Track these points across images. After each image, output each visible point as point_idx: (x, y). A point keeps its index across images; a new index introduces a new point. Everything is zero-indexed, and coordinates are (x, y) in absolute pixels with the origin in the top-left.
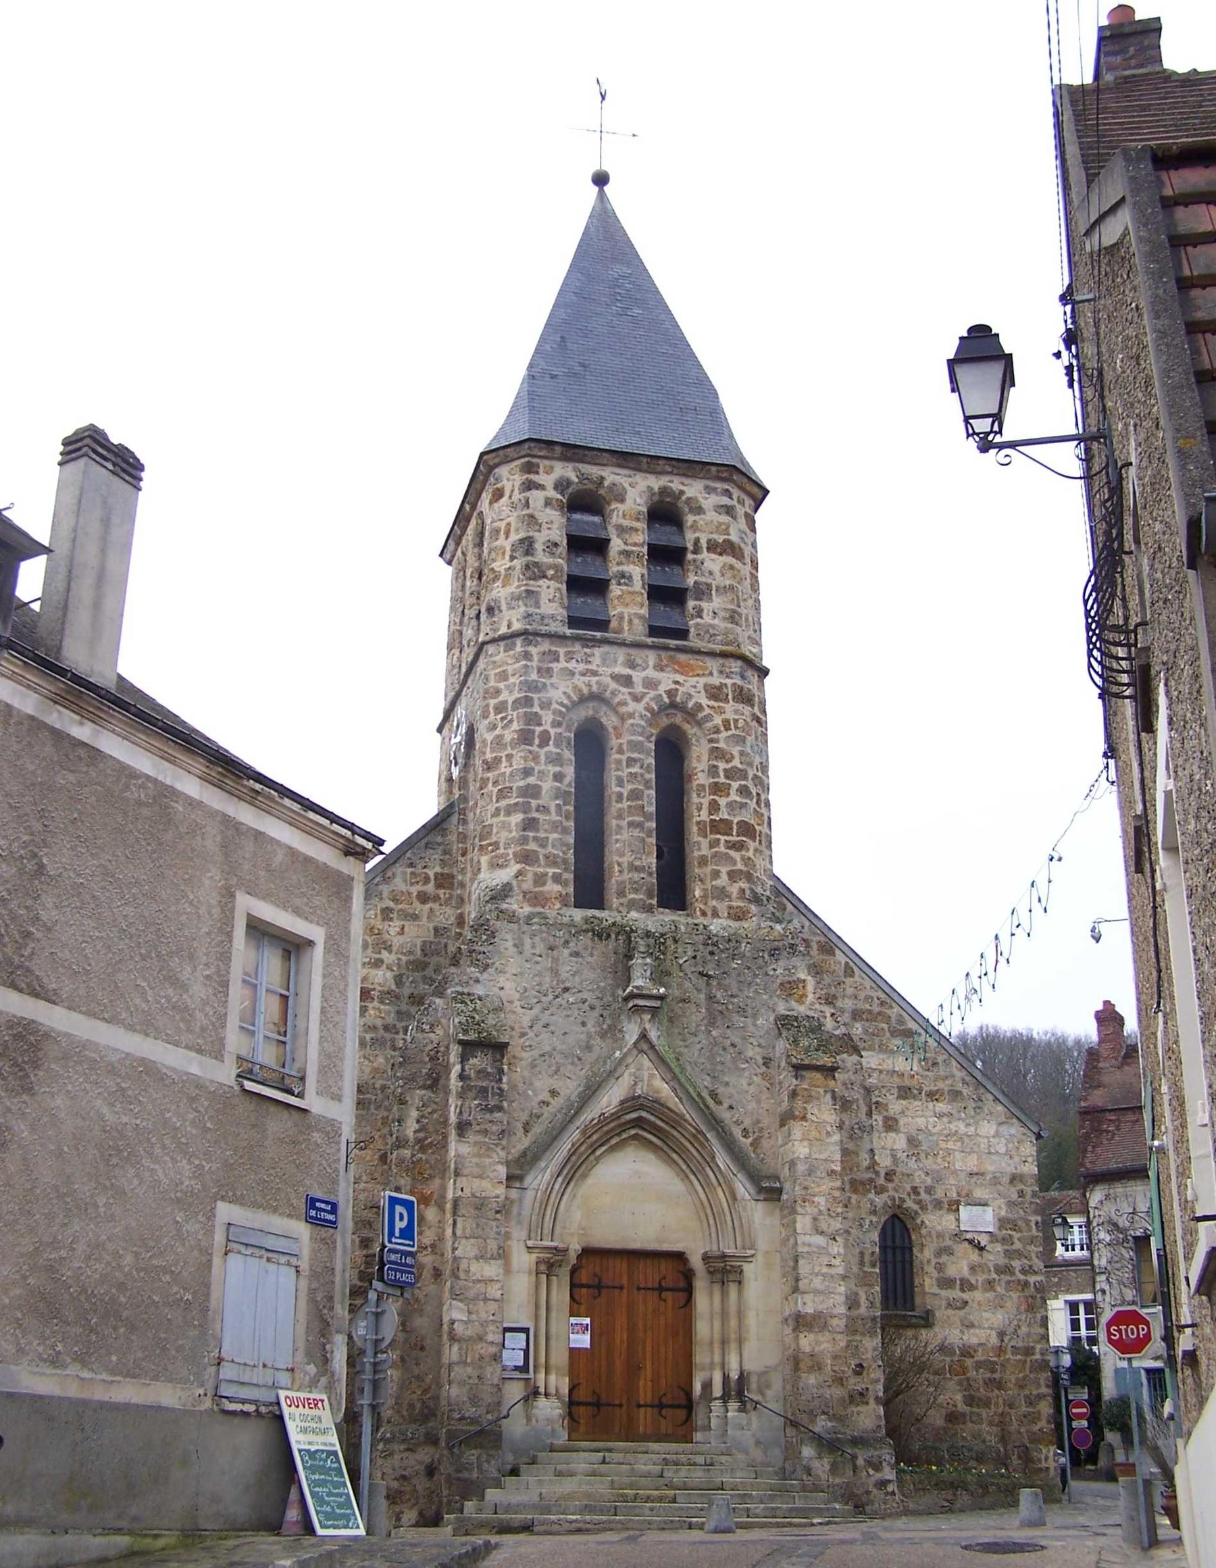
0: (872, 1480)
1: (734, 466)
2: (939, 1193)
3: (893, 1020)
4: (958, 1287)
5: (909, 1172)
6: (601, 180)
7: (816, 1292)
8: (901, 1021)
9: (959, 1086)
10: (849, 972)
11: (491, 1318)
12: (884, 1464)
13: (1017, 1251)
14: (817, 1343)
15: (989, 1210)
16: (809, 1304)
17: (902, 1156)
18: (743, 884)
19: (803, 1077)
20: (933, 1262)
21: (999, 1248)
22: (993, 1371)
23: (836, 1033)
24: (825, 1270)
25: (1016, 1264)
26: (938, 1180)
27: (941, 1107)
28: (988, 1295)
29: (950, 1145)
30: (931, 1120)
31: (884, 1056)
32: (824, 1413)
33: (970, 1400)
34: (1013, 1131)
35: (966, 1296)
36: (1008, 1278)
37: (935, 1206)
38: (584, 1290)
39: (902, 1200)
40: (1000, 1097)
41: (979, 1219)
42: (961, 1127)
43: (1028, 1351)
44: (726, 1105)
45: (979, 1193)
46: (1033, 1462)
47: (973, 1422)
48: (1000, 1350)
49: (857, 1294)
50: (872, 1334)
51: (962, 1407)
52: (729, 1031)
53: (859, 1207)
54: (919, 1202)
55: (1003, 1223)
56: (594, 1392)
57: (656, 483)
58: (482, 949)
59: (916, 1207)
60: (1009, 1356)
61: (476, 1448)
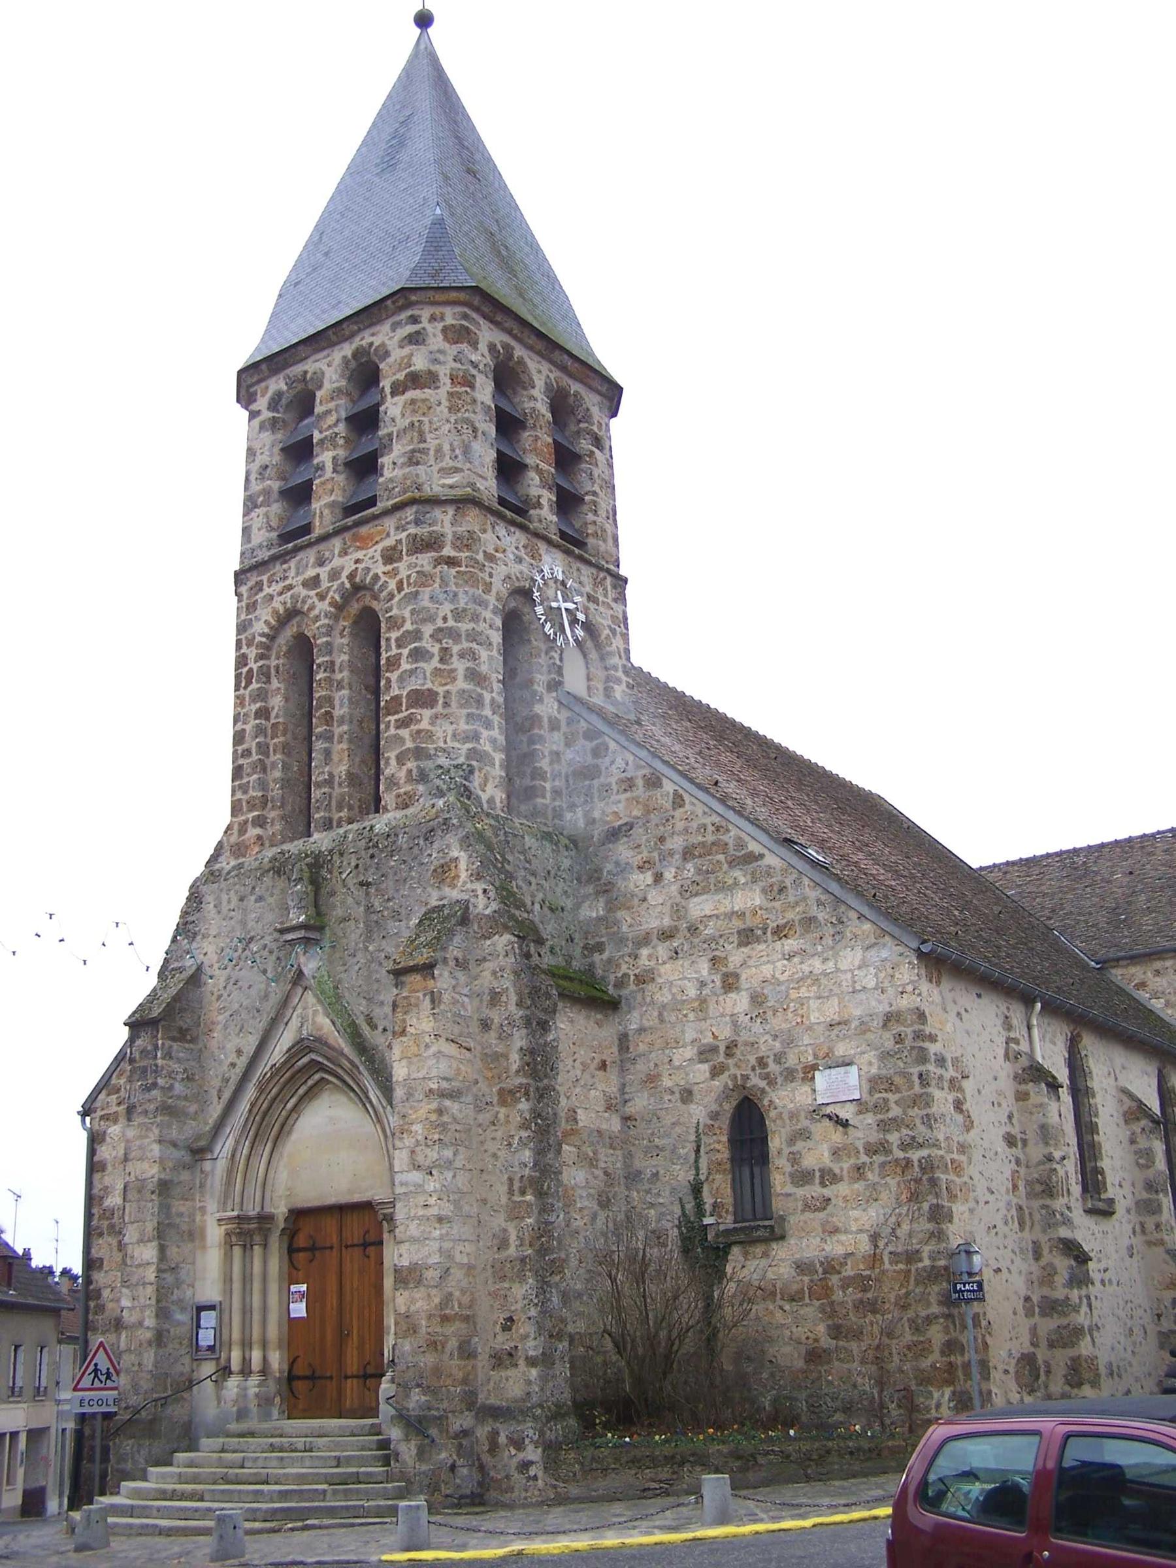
0: (514, 1462)
1: (403, 289)
2: (791, 1061)
3: (731, 847)
4: (817, 1181)
6: (424, 20)
7: (413, 1240)
8: (740, 844)
9: (814, 911)
11: (148, 1302)
12: (527, 1441)
13: (894, 1119)
14: (413, 1301)
15: (854, 1069)
16: (405, 1255)
18: (411, 765)
19: (403, 983)
20: (786, 1151)
21: (870, 1119)
22: (865, 1290)
23: (487, 912)
24: (421, 1213)
25: (894, 1138)
26: (790, 1042)
27: (791, 944)
28: (856, 1186)
29: (804, 992)
30: (779, 964)
31: (721, 896)
32: (418, 1386)
33: (836, 1332)
34: (884, 954)
35: (826, 1192)
36: (882, 1159)
37: (786, 1078)
38: (301, 1254)
39: (746, 1078)
40: (865, 911)
41: (839, 1086)
42: (817, 965)
43: (912, 1257)
44: (380, 1028)
45: (842, 1050)
46: (918, 1411)
47: (839, 1360)
48: (874, 1259)
49: (505, 1230)
50: (522, 1279)
51: (826, 1342)
52: (384, 942)
53: (508, 1122)
54: (766, 1077)
55: (875, 1083)
56: (310, 1365)
57: (347, 349)
58: (193, 918)
59: (763, 1084)
61: (131, 1438)
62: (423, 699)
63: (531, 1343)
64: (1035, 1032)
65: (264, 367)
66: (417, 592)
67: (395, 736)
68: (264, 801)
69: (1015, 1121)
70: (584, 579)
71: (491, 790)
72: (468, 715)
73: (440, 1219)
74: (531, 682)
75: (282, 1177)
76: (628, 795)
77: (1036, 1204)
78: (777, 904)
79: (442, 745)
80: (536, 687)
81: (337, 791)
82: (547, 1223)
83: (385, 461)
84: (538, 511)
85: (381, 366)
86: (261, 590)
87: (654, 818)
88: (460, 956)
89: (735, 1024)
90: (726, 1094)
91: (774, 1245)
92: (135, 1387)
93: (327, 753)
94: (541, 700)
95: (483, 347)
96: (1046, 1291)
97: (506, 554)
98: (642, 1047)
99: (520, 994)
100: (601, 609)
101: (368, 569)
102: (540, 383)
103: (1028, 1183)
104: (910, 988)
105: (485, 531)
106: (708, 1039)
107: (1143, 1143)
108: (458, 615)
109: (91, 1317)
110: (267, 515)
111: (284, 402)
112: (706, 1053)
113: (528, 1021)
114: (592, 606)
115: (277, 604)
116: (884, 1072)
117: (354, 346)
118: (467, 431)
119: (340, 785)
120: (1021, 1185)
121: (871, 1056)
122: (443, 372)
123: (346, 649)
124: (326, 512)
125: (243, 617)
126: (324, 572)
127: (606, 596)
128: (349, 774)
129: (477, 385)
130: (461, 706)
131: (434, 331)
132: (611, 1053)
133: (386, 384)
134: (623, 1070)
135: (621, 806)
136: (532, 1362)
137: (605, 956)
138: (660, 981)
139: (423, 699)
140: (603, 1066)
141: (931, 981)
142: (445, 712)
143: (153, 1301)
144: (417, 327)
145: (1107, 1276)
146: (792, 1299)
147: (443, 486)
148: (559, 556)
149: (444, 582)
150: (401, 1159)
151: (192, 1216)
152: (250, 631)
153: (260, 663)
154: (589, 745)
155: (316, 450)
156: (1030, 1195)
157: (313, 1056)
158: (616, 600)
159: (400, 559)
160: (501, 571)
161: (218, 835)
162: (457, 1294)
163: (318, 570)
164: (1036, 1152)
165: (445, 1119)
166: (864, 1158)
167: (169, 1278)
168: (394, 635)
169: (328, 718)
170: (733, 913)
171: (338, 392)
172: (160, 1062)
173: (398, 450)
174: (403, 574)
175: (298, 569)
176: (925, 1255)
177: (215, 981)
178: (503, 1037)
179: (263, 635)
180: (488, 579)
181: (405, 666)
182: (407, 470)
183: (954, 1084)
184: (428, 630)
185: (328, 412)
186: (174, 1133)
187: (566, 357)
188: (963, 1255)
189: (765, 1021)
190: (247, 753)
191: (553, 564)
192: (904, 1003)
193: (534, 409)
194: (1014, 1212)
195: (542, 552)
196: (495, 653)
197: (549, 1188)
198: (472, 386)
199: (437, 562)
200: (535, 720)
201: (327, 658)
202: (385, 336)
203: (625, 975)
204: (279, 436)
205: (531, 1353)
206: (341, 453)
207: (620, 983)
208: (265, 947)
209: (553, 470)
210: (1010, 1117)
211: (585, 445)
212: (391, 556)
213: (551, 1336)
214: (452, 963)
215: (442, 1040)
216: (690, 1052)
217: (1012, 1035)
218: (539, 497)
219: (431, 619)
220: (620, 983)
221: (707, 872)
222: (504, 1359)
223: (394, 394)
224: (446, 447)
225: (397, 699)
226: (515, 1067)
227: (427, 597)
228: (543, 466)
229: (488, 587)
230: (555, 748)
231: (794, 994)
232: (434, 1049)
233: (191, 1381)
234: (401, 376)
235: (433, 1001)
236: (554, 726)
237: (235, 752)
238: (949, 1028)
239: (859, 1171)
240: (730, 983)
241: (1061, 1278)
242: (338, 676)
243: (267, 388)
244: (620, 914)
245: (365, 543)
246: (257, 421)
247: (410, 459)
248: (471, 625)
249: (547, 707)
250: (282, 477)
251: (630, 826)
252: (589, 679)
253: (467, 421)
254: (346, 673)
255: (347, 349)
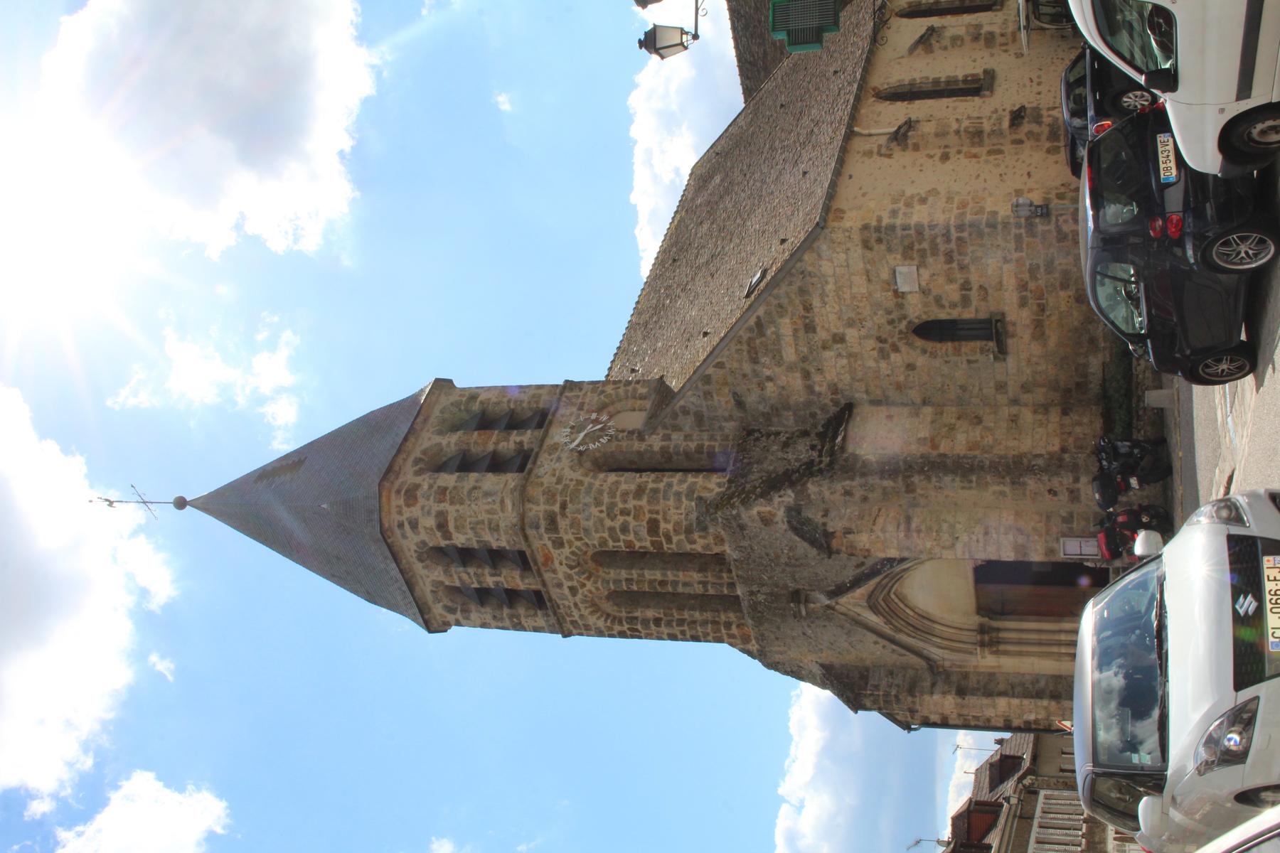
2: (890, 304)
8: (750, 329)
9: (795, 287)
15: (899, 269)
20: (948, 310)
21: (930, 260)
25: (942, 247)
27: (816, 303)
29: (847, 296)
35: (975, 287)
41: (908, 277)
45: (885, 275)
54: (900, 320)
55: (907, 255)
62: (653, 527)
64: (873, 131)
68: (715, 623)
69: (932, 153)
71: (712, 486)
73: (986, 533)
74: (639, 452)
75: (956, 619)
77: (986, 140)
78: (790, 309)
81: (710, 579)
82: (990, 467)
83: (495, 545)
87: (730, 379)
89: (866, 337)
91: (1008, 319)
93: (685, 584)
94: (650, 446)
95: (418, 480)
98: (879, 392)
99: (845, 479)
102: (438, 439)
103: (973, 145)
105: (542, 484)
106: (875, 353)
107: (946, 42)
108: (598, 503)
110: (527, 617)
111: (450, 604)
112: (883, 355)
114: (586, 407)
115: (586, 612)
116: (900, 251)
118: (475, 493)
121: (890, 258)
122: (436, 507)
126: (567, 584)
128: (700, 571)
131: (408, 513)
133: (443, 543)
136: (1077, 480)
137: (819, 412)
139: (653, 527)
146: (1043, 310)
149: (578, 511)
151: (979, 674)
154: (681, 417)
155: (484, 585)
156: (981, 144)
158: (581, 389)
160: (568, 474)
161: (735, 652)
164: (952, 139)
165: (923, 527)
166: (955, 265)
167: (1018, 689)
168: (611, 543)
171: (445, 572)
174: (571, 537)
177: (828, 657)
178: (872, 488)
181: (631, 537)
184: (608, 523)
185: (460, 578)
186: (927, 684)
189: (864, 319)
190: (683, 633)
191: (559, 435)
192: (856, 237)
194: (991, 158)
196: (622, 479)
198: (446, 489)
199: (564, 515)
200: (664, 450)
202: (409, 544)
203: (832, 400)
206: (487, 571)
207: (836, 403)
210: (930, 157)
212: (559, 544)
215: (875, 528)
216: (883, 365)
217: (875, 150)
219: (601, 521)
220: (836, 403)
225: (653, 543)
229: (580, 483)
231: (848, 302)
232: (880, 534)
234: (439, 534)
236: (667, 438)
238: (872, 205)
239: (962, 268)
240: (839, 339)
242: (635, 576)
244: (792, 403)
245: (548, 559)
246: (462, 621)
248: (605, 495)
249: (656, 442)
250: (500, 607)
251: (735, 394)
252: (634, 410)
253: (470, 492)
255: (418, 568)
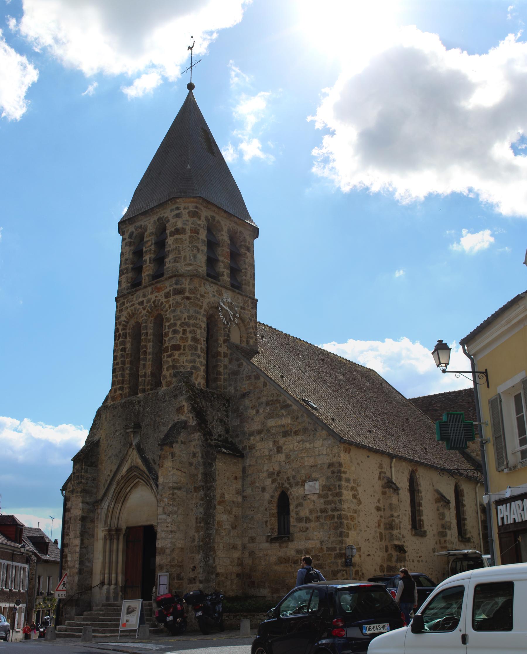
3: (281, 401)
5: (285, 471)
6: (191, 87)
7: (162, 539)
8: (285, 401)
10: (265, 385)
14: (162, 559)
17: (283, 464)
21: (322, 500)
24: (165, 529)
25: (329, 507)
27: (299, 438)
29: (303, 455)
30: (295, 444)
35: (307, 525)
41: (313, 488)
45: (314, 475)
49: (194, 536)
54: (289, 484)
57: (155, 218)
59: (288, 486)
60: (325, 552)
62: (176, 347)
63: (200, 575)
64: (393, 469)
65: (127, 222)
66: (175, 309)
67: (166, 360)
68: (123, 382)
70: (240, 301)
71: (199, 380)
72: (192, 353)
74: (217, 340)
75: (124, 516)
76: (248, 382)
79: (182, 364)
80: (219, 341)
81: (148, 379)
83: (167, 260)
84: (222, 277)
85: (167, 225)
86: (124, 305)
88: (183, 440)
89: (280, 465)
90: (276, 489)
91: (290, 543)
92: (72, 589)
93: (144, 365)
94: (221, 346)
95: (203, 218)
96: (389, 563)
97: (209, 292)
98: (250, 472)
100: (246, 312)
101: (160, 300)
102: (225, 229)
103: (385, 524)
104: (337, 454)
105: (200, 287)
106: (271, 470)
107: (441, 510)
108: (189, 317)
109: (63, 564)
110: (127, 277)
112: (270, 475)
113: (204, 463)
114: (242, 311)
115: (129, 310)
116: (327, 484)
117: (158, 217)
119: (148, 377)
120: (382, 525)
122: (188, 228)
123: (152, 328)
124: (147, 278)
125: (118, 314)
126: (145, 300)
127: (248, 306)
128: (152, 373)
129: (200, 233)
130: (190, 350)
132: (239, 474)
133: (168, 232)
134: (243, 480)
135: (246, 385)
136: (201, 582)
137: (239, 439)
138: (257, 448)
139: (176, 347)
140: (236, 478)
141: (345, 452)
142: (184, 352)
143: (78, 559)
144: (179, 211)
145: (420, 559)
146: (294, 563)
147: (186, 270)
148: (230, 293)
150: (160, 510)
152: (120, 320)
153: (123, 331)
155: (144, 254)
156: (385, 529)
157: (135, 473)
159: (170, 297)
160: (206, 301)
162: (177, 558)
163: (143, 299)
165: (175, 497)
166: (319, 514)
167: (84, 550)
168: (167, 324)
169: (145, 353)
170: (281, 425)
171: (152, 233)
172: (83, 474)
173: (171, 257)
175: (136, 298)
176: (338, 549)
177: (103, 445)
179: (124, 321)
180: (201, 304)
181: (171, 336)
182: (173, 264)
183: (352, 489)
184: (179, 323)
185: (148, 241)
186: (88, 500)
187: (236, 219)
188: (350, 549)
191: (227, 296)
192: (335, 460)
193: (223, 239)
194: (378, 535)
195: (223, 292)
196: (203, 331)
197: (210, 521)
198: (198, 234)
200: (218, 354)
201: (145, 331)
203: (246, 446)
204: (132, 248)
205: (200, 579)
206: (152, 256)
208: (121, 434)
209: (229, 262)
211: (243, 250)
212: (167, 296)
213: (208, 573)
214: (179, 442)
215: (175, 470)
216: (265, 474)
217: (383, 470)
218: (223, 272)
219: (180, 319)
220: (244, 448)
221: (273, 410)
222: (192, 581)
223: (170, 236)
224: (188, 256)
225: (167, 347)
226: (200, 479)
227: (179, 311)
228: (225, 260)
229: (201, 307)
230: (225, 364)
232: (171, 473)
233: (91, 587)
234: (173, 229)
235: (172, 456)
236: (225, 355)
237: (113, 363)
238: (353, 468)
239: (318, 518)
240: (279, 450)
241: (394, 559)
242: (149, 338)
243: (128, 230)
245: (159, 290)
246: (124, 242)
247: (175, 261)
248: (194, 321)
249: (223, 349)
250: (132, 263)
252: (241, 337)
254: (151, 337)
